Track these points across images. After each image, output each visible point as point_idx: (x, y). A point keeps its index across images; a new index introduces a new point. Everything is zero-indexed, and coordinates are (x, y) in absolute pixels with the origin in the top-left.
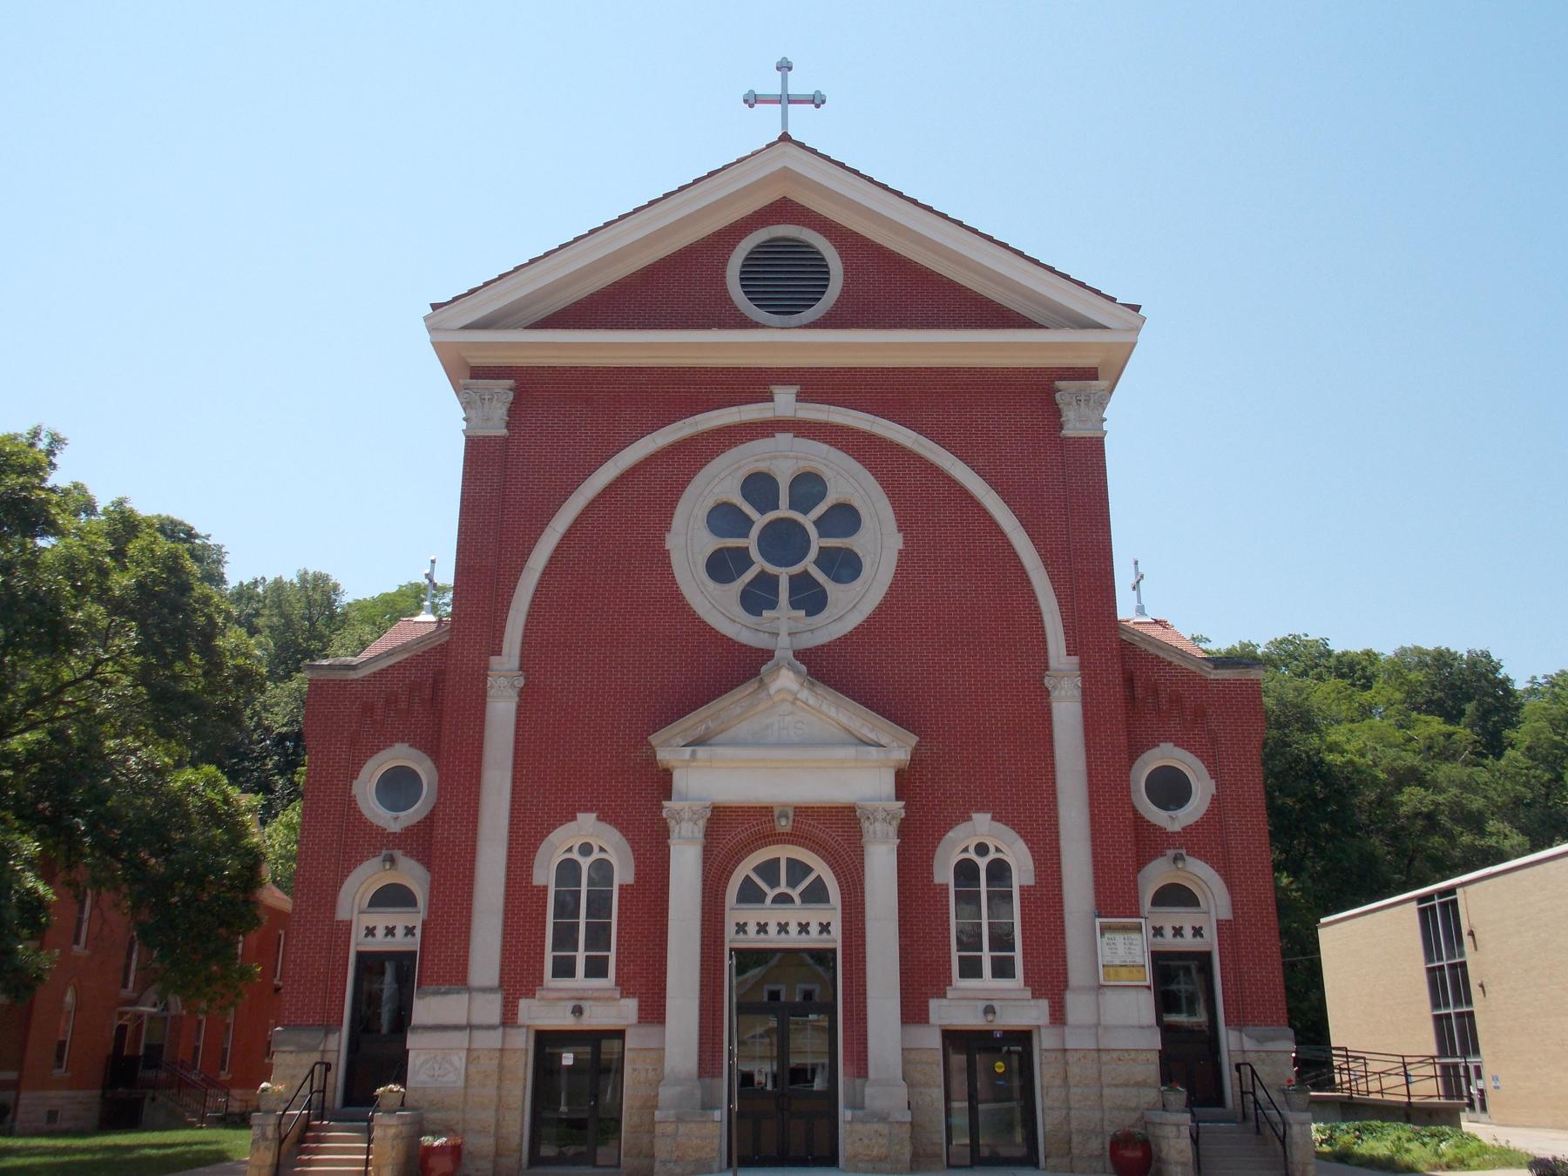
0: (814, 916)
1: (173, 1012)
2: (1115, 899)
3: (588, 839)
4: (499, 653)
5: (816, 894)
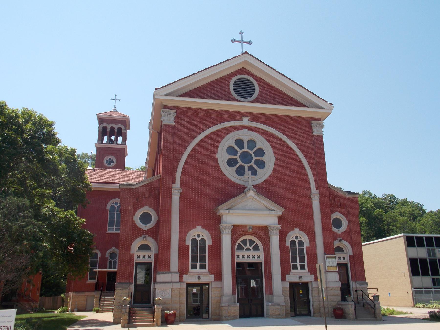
0: (256, 254)
2: (330, 250)
3: (199, 232)
4: (175, 183)
5: (256, 248)
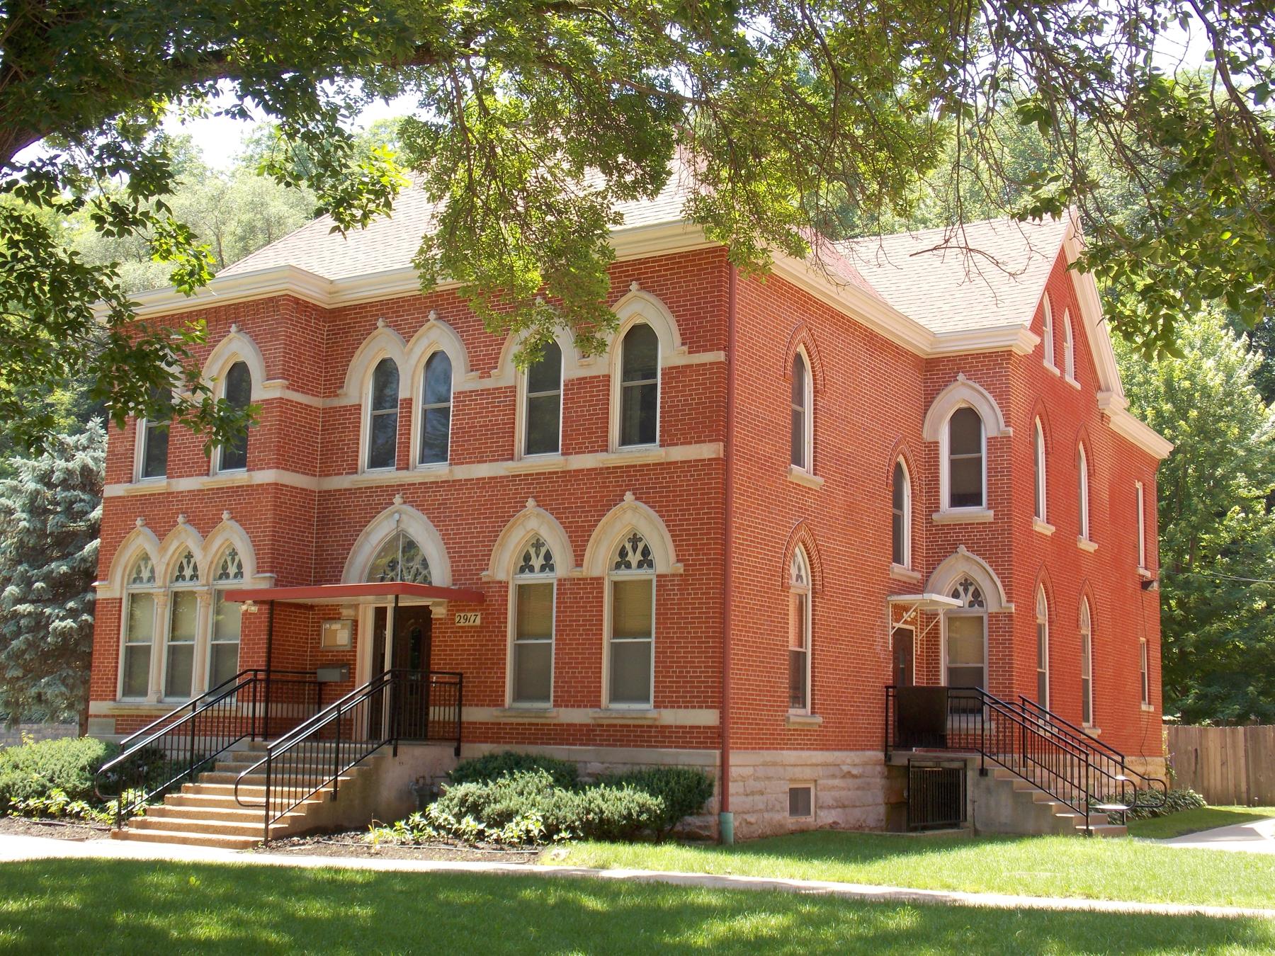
1: (992, 606)
